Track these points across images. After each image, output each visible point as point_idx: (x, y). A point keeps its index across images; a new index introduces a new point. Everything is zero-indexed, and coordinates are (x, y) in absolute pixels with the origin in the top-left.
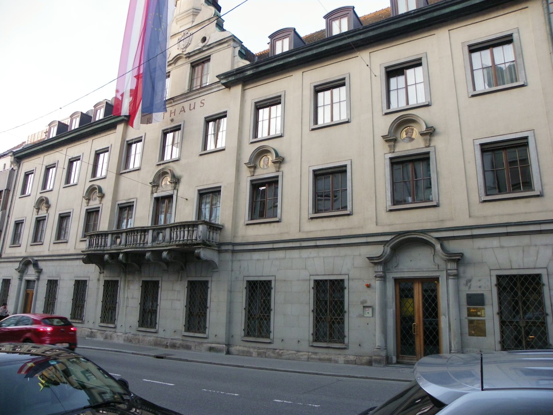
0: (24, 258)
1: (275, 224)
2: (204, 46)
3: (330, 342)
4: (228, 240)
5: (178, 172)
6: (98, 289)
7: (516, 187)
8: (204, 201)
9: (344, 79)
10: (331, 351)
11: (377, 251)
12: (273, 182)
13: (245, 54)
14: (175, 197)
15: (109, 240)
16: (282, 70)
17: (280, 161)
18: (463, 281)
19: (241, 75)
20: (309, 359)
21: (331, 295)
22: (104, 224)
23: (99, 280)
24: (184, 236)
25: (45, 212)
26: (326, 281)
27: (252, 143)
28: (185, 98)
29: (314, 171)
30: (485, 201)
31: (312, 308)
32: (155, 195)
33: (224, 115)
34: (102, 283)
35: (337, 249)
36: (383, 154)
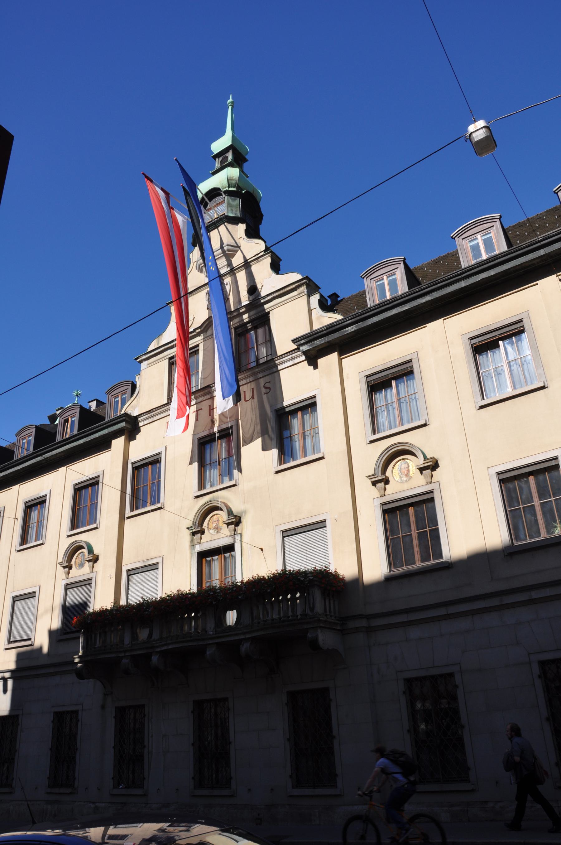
14: (237, 547)
23: (103, 707)
32: (198, 548)
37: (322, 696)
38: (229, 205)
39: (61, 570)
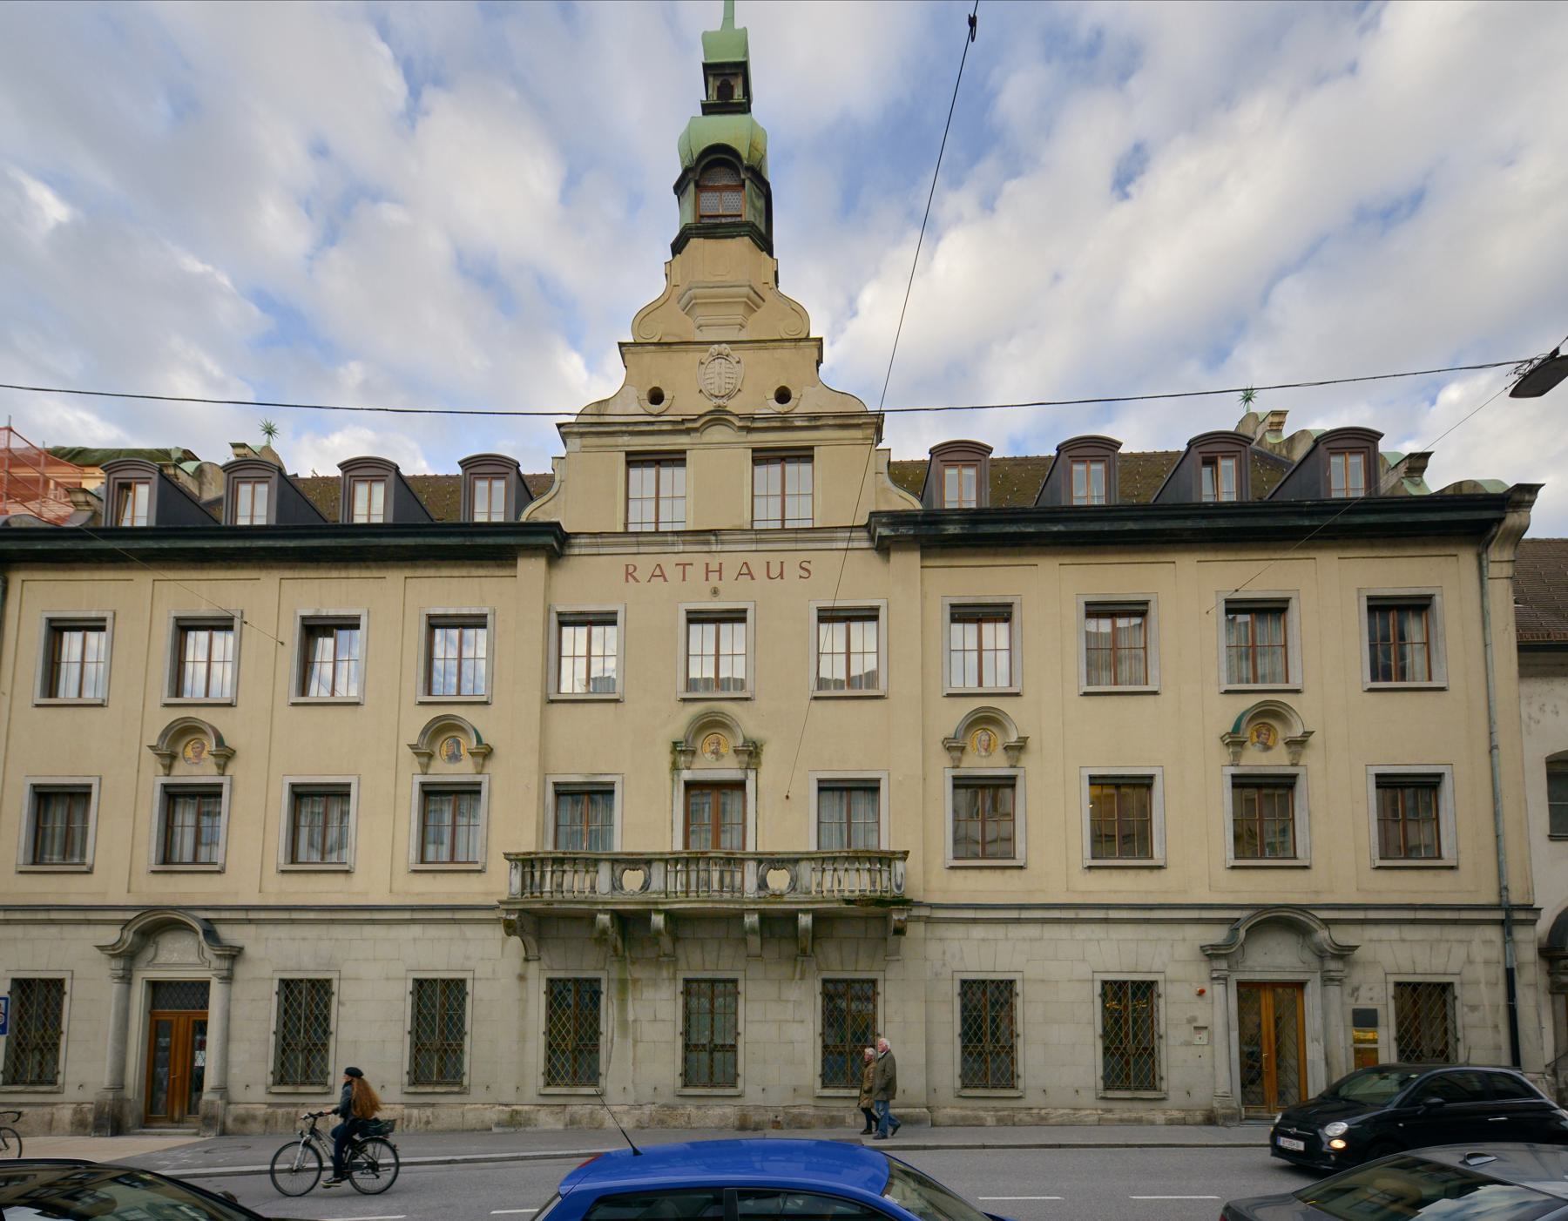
1: (1015, 872)
11: (1218, 935)
17: (225, 756)
19: (932, 531)
20: (1100, 1122)
23: (522, 978)
25: (214, 770)
28: (751, 541)
30: (1379, 868)
32: (687, 775)
33: (351, 624)
35: (1144, 927)
36: (154, 780)
37: (867, 990)
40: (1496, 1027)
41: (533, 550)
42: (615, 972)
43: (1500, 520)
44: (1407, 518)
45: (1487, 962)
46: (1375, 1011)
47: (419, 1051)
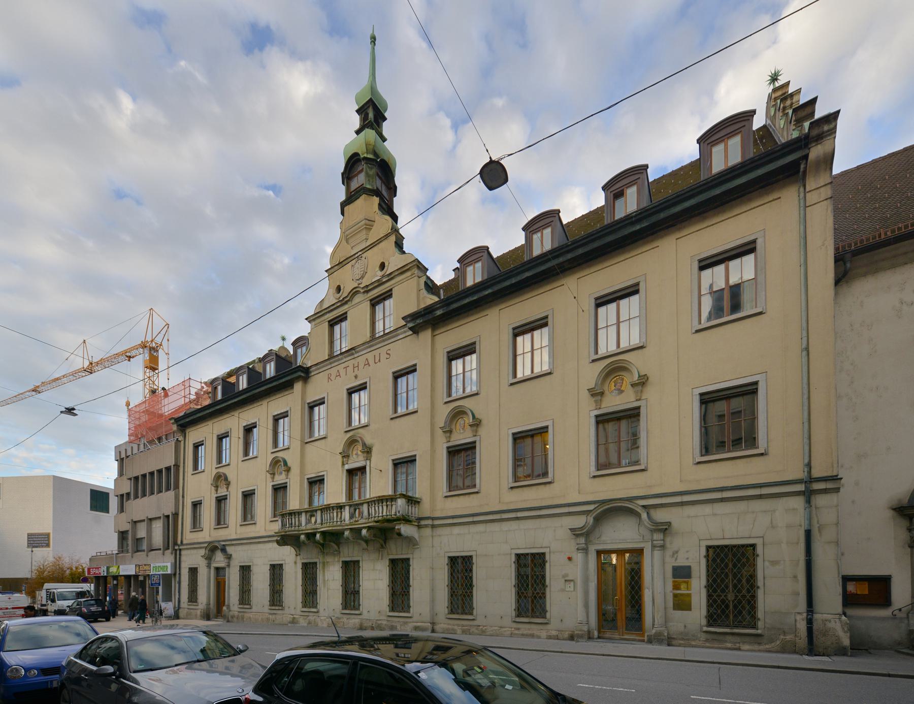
0: (210, 543)
2: (383, 276)
3: (533, 617)
4: (427, 514)
5: (368, 441)
6: (296, 572)
7: (736, 443)
8: (399, 471)
9: (546, 317)
10: (533, 626)
11: (579, 522)
12: (471, 448)
13: (431, 287)
15: (303, 518)
16: (476, 308)
18: (669, 553)
19: (430, 317)
20: (512, 635)
21: (532, 569)
22: (295, 500)
23: (295, 563)
24: (382, 511)
26: (527, 554)
27: (446, 403)
29: (514, 434)
31: (514, 583)
32: (347, 467)
34: (300, 566)
35: (538, 521)
38: (367, 175)
39: (269, 475)
40: (795, 577)
41: (298, 378)
42: (321, 557)
43: (806, 157)
44: (717, 191)
45: (789, 526)
46: (689, 567)
47: (520, 597)
